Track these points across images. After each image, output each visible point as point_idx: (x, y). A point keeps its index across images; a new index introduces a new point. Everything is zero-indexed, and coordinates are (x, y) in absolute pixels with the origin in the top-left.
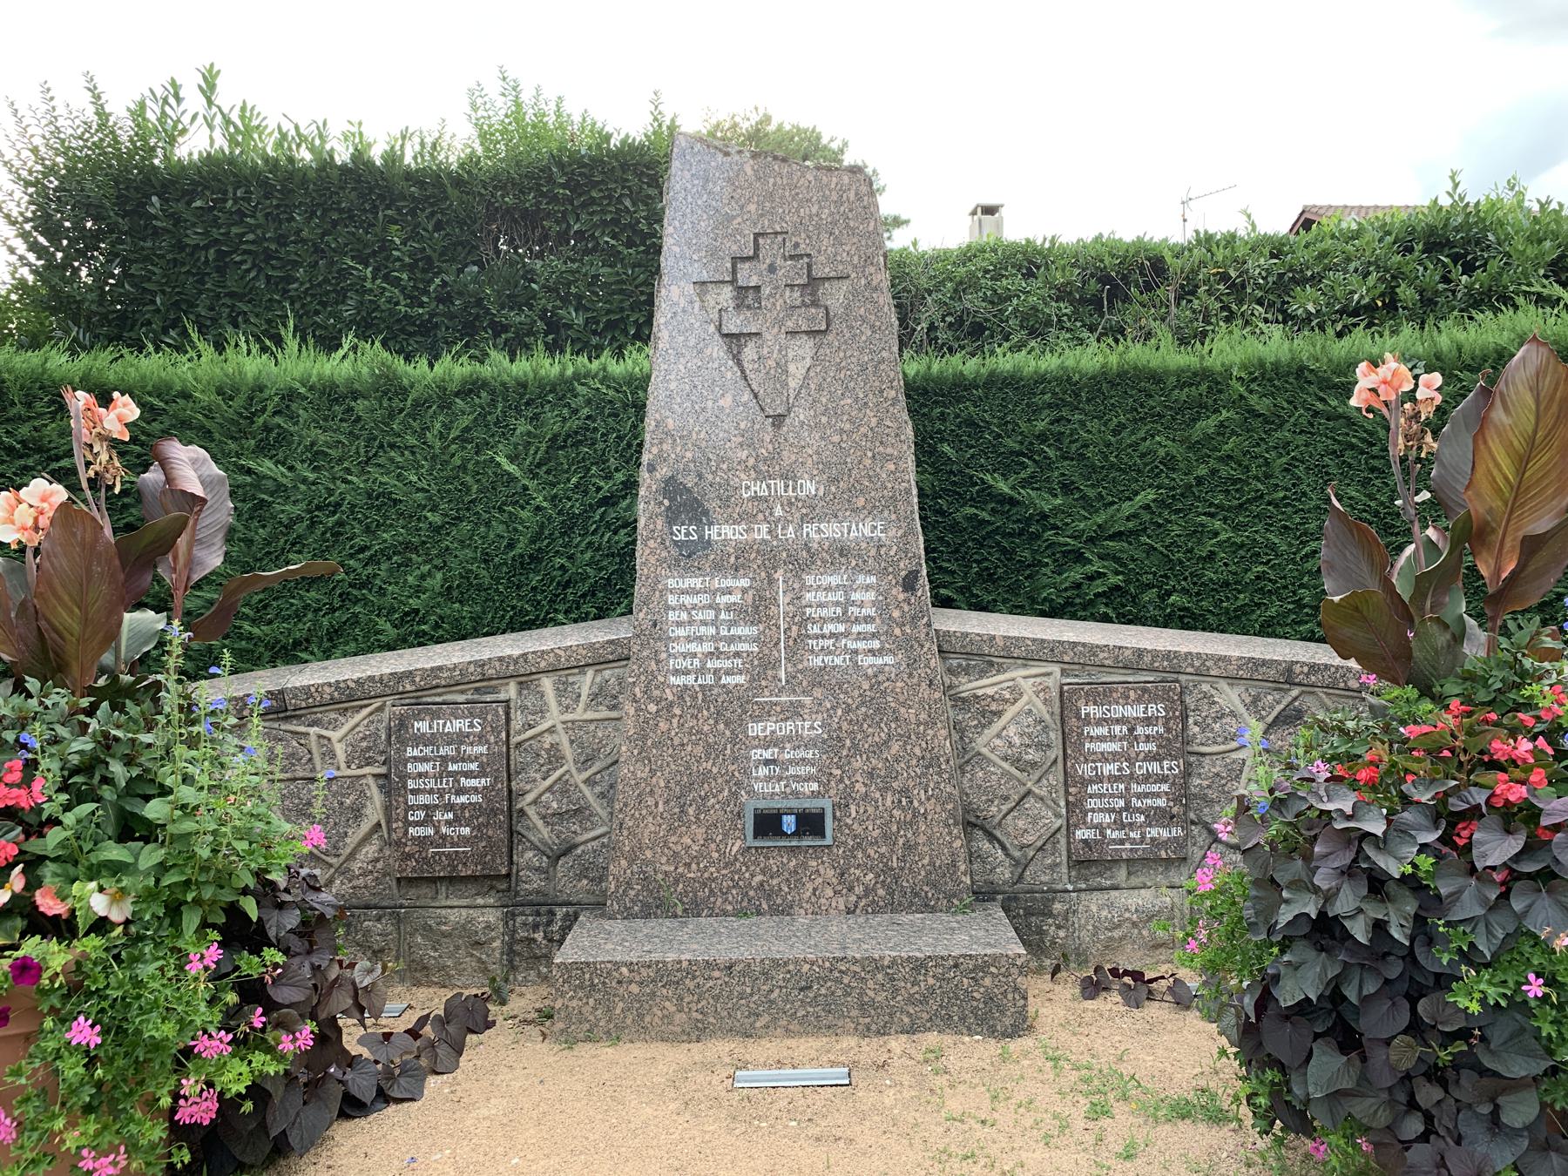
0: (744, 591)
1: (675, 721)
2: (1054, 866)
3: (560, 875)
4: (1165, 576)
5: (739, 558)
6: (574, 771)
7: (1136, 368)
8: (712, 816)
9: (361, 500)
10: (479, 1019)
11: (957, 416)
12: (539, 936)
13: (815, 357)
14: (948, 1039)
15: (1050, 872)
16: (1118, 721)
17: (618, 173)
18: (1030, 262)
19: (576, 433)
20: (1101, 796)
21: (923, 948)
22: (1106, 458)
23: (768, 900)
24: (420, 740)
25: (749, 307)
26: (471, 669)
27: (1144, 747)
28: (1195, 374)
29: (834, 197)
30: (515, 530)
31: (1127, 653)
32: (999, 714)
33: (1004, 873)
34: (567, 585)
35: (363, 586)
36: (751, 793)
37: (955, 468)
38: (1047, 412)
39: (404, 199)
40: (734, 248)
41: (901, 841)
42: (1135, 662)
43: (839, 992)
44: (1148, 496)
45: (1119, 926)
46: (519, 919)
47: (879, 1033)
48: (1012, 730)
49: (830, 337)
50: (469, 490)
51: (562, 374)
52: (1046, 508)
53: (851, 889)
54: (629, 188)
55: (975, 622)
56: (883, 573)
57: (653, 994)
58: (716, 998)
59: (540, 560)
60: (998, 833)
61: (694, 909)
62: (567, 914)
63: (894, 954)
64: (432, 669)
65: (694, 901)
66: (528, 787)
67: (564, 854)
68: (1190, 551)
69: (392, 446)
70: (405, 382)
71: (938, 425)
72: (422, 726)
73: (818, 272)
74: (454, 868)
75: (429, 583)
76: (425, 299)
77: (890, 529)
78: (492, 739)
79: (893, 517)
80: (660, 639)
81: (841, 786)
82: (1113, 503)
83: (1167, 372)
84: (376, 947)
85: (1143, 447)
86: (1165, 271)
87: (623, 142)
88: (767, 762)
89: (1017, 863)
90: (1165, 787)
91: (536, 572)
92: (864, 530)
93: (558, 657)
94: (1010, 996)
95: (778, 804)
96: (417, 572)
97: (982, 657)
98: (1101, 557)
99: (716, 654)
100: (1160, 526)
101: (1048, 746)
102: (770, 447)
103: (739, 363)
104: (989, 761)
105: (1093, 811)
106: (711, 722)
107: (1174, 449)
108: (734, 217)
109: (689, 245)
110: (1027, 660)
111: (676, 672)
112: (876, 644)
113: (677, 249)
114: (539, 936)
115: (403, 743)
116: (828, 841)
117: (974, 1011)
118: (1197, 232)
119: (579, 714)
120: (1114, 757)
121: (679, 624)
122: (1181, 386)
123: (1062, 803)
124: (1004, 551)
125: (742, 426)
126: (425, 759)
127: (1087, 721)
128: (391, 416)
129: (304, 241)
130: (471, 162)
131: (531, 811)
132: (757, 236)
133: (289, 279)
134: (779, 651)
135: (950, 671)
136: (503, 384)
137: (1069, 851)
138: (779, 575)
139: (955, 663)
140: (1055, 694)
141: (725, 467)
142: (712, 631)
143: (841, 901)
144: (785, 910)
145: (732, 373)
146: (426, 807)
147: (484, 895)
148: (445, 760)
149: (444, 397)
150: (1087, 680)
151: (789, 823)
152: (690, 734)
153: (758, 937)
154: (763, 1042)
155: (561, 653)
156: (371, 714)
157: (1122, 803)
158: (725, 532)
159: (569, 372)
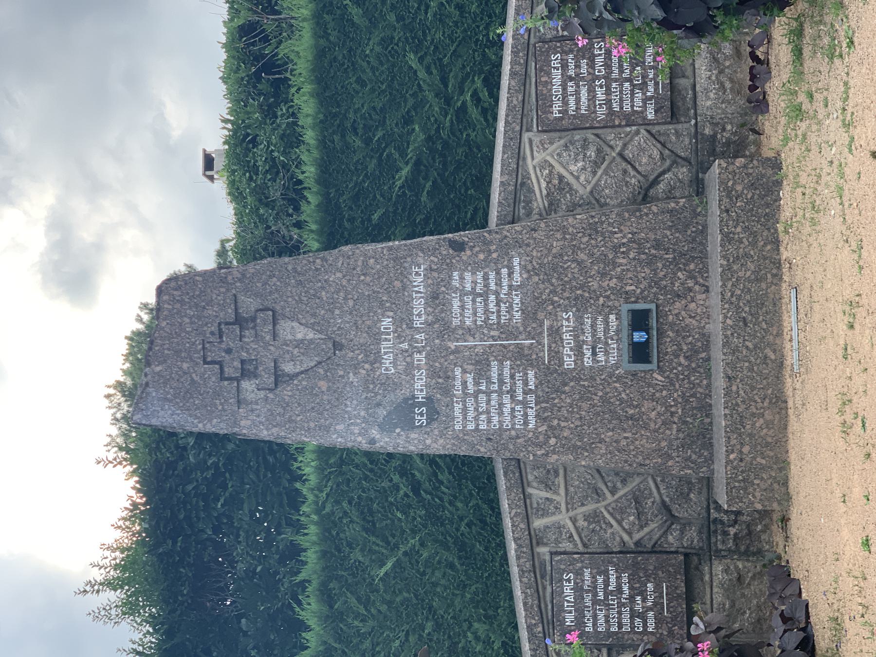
0: (464, 371)
1: (563, 424)
2: (677, 134)
3: (686, 515)
5: (441, 378)
6: (604, 503)
7: (313, 70)
8: (635, 395)
11: (351, 208)
12: (732, 531)
16: (565, 89)
18: (244, 140)
19: (362, 513)
20: (621, 100)
22: (384, 91)
25: (256, 368)
26: (525, 580)
27: (584, 69)
28: (318, 23)
29: (178, 306)
30: (439, 562)
31: (513, 83)
32: (561, 178)
33: (683, 172)
34: (483, 521)
36: (617, 366)
37: (391, 209)
38: (348, 138)
40: (214, 379)
41: (653, 251)
42: (522, 78)
43: (748, 297)
44: (412, 59)
46: (720, 546)
49: (278, 308)
51: (316, 523)
52: (422, 137)
53: (690, 290)
54: (177, 486)
56: (451, 267)
57: (751, 435)
58: (753, 388)
60: (652, 178)
62: (714, 509)
64: (525, 610)
65: (699, 409)
66: (618, 539)
68: (456, 23)
70: (321, 648)
71: (358, 223)
73: (232, 317)
74: (679, 596)
75: (482, 634)
77: (418, 264)
78: (579, 565)
79: (409, 259)
80: (500, 435)
81: (612, 297)
82: (419, 85)
87: (139, 491)
88: (594, 354)
89: (674, 162)
91: (474, 546)
93: (516, 514)
94: (751, 171)
96: (473, 643)
98: (462, 92)
99: (512, 392)
100: (436, 48)
101: (585, 140)
102: (357, 352)
104: (597, 184)
105: (632, 106)
106: (563, 396)
107: (375, 39)
108: (192, 379)
111: (526, 423)
112: (504, 271)
114: (732, 531)
116: (653, 307)
117: (762, 197)
119: (561, 498)
120: (591, 91)
121: (489, 421)
122: (326, 35)
123: (628, 129)
125: (341, 373)
126: (595, 617)
127: (564, 112)
130: (153, 620)
131: (637, 536)
134: (510, 345)
135: (529, 214)
136: (323, 569)
138: (452, 345)
139: (522, 211)
141: (371, 386)
142: (494, 395)
143: (699, 297)
146: (632, 618)
147: (703, 574)
148: (595, 602)
149: (333, 617)
150: (535, 113)
151: (639, 337)
155: (514, 511)
157: (627, 84)
159: (315, 517)
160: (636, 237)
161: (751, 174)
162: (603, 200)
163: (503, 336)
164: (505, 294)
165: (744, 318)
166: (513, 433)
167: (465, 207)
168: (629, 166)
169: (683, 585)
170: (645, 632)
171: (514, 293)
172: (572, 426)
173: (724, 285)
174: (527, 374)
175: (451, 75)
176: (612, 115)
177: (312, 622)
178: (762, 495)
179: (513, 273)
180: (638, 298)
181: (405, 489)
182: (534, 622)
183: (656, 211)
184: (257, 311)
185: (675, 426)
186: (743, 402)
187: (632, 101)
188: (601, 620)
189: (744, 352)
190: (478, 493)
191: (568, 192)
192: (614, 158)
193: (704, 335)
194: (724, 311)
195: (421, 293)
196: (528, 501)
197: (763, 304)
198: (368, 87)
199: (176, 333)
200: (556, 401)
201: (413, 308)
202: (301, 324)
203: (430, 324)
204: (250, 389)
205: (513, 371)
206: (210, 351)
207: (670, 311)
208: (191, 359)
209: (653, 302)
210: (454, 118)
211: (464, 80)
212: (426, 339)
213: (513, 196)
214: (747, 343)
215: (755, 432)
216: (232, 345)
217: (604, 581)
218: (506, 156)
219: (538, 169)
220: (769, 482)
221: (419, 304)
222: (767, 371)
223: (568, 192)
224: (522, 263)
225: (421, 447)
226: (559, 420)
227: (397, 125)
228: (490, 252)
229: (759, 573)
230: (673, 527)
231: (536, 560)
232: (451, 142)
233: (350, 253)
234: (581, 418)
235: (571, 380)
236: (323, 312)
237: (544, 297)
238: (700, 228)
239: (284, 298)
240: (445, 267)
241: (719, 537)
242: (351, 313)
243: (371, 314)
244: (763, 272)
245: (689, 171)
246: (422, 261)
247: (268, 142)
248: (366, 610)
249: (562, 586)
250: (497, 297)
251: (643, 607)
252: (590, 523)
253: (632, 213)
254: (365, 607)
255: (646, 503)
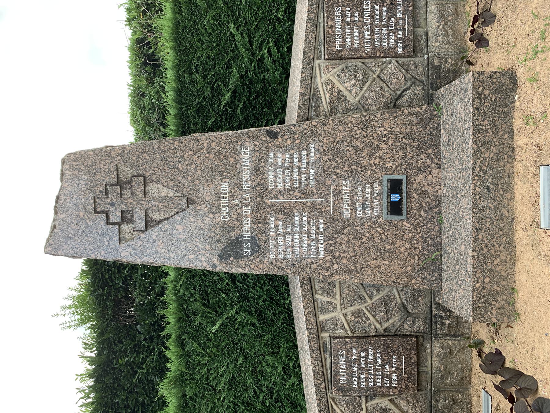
0: (277, 219)
1: (342, 255)
2: (415, 65)
4: (270, 20)
5: (261, 222)
6: (365, 305)
8: (391, 236)
9: (233, 393)
10: (497, 358)
12: (447, 322)
13: (158, 182)
14: (517, 114)
15: (418, 66)
16: (343, 31)
17: (98, 267)
19: (202, 294)
20: (381, 40)
21: (466, 127)
23: (433, 208)
24: (349, 381)
25: (132, 216)
26: (314, 355)
27: (357, 18)
28: (175, 5)
30: (246, 323)
31: (309, 26)
32: (339, 91)
33: (418, 90)
34: (272, 299)
35: (272, 393)
39: (109, 356)
41: (405, 140)
42: (313, 21)
43: (491, 172)
44: (232, 27)
45: (446, 31)
47: (513, 151)
48: (347, 85)
49: (147, 175)
50: (228, 344)
51: (175, 301)
52: (237, 75)
53: (428, 166)
55: (293, 104)
56: (268, 149)
57: (490, 270)
58: (493, 237)
59: (261, 311)
60: (399, 92)
61: (437, 246)
62: (436, 308)
63: (471, 142)
64: (314, 375)
65: (433, 246)
66: (373, 327)
67: (406, 309)
69: (207, 379)
70: (178, 373)
72: (342, 380)
73: (114, 181)
74: (413, 364)
75: (270, 362)
76: (151, 347)
77: (246, 146)
78: (350, 345)
79: (239, 143)
80: (301, 262)
81: (377, 171)
83: (175, 18)
84: (452, 403)
85: (209, 30)
86: (142, 38)
87: (85, 264)
88: (364, 208)
90: (377, 7)
92: (246, 159)
94: (495, 80)
95: (385, 203)
96: (266, 367)
97: (310, 99)
98: (261, 50)
99: (308, 233)
100: (246, 23)
101: (355, 66)
102: (204, 206)
103: (161, 221)
104: (363, 96)
105: (388, 44)
106: (343, 236)
108: (87, 223)
109: (100, 246)
110: (312, 76)
111: (318, 254)
112: (304, 153)
113: (103, 253)
114: (447, 322)
115: (351, 389)
116: (404, 177)
117: (502, 100)
118: (126, 25)
120: (361, 33)
123: (384, 60)
124: (257, 96)
125: (193, 220)
126: (359, 378)
127: (343, 46)
128: (194, 379)
129: (127, 398)
131: (385, 325)
132: (96, 212)
133: (143, 404)
134: (307, 202)
135: (317, 116)
136: (179, 328)
137: (408, 57)
138: (269, 202)
139: (313, 113)
140: (329, 63)
141: (214, 229)
142: (297, 236)
143: (434, 171)
144: (439, 201)
145: (165, 225)
146: (383, 378)
148: (359, 369)
149: (185, 356)
151: (395, 197)
152: (349, 247)
153: (456, 215)
154: (517, 212)
155: (307, 311)
156: (336, 404)
157: (385, 29)
158: (247, 229)
160: (393, 130)
161: (495, 83)
162: (366, 107)
163: (303, 196)
164: (304, 168)
165: (488, 187)
166: (309, 260)
167: (262, 119)
168: (385, 84)
169: (415, 356)
170: (391, 387)
171: (310, 167)
172: (349, 256)
173: (475, 163)
174: (318, 221)
175: (255, 39)
176: (375, 49)
177: (173, 369)
178: (497, 312)
179: (310, 154)
180: (394, 172)
181: (227, 281)
182: (319, 382)
183: (407, 113)
184: (133, 176)
185: (417, 257)
186: (486, 246)
187: (388, 40)
188: (363, 379)
189: (488, 211)
190: (269, 283)
191: (343, 101)
192: (375, 79)
193: (437, 197)
194: (474, 182)
195: (247, 166)
196: (316, 303)
197: (501, 177)
198: (206, 44)
199: (75, 191)
200: (338, 240)
201: (242, 176)
202: (164, 186)
203: (254, 187)
204: (128, 230)
205: (309, 219)
206: (99, 204)
207: (415, 180)
208: (85, 209)
209: (404, 174)
210: (256, 65)
211: (261, 44)
212: (251, 198)
213: (308, 103)
214: (489, 204)
215: (493, 268)
216: (115, 200)
217: (365, 355)
218: (304, 75)
219: (324, 85)
220: (502, 303)
221: (247, 174)
222: (503, 225)
223: (343, 101)
224: (316, 147)
225: (247, 270)
226: (340, 252)
227: (222, 68)
228: (295, 139)
229: (462, 348)
230: (408, 319)
231: (321, 341)
232: (254, 80)
233: (199, 138)
234: (354, 251)
235: (348, 226)
236: (180, 178)
237: (330, 170)
238: (436, 125)
239: (152, 168)
240: (264, 149)
241: (438, 326)
242: (199, 179)
243: (213, 180)
244: (501, 154)
245: (423, 89)
246: (248, 145)
247: (150, 95)
248: (204, 351)
249: (338, 359)
250: (299, 170)
251: (390, 371)
252: (355, 317)
253: (391, 115)
254: (204, 349)
255: (391, 304)
